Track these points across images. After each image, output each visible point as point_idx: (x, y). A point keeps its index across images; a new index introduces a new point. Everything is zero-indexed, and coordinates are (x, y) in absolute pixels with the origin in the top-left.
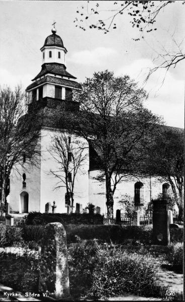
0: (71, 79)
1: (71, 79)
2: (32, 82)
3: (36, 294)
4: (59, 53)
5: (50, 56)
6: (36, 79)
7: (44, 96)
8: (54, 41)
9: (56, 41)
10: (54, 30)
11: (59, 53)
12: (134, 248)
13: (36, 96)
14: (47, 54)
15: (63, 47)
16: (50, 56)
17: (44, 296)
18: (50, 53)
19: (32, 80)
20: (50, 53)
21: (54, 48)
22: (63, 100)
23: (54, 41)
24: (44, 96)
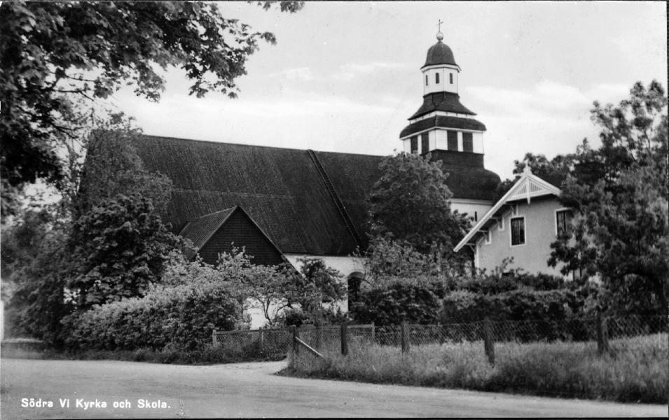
0: (469, 117)
1: (469, 117)
2: (407, 123)
3: (45, 403)
4: (451, 75)
5: (437, 81)
6: (414, 117)
7: (431, 148)
8: (440, 56)
9: (9, 295)
10: (440, 35)
11: (451, 75)
12: (415, 398)
13: (423, 142)
14: (432, 79)
15: (455, 65)
16: (437, 81)
17: (63, 405)
18: (437, 75)
19: (410, 119)
20: (437, 75)
21: (429, 69)
22: (461, 153)
23: (440, 56)
24: (431, 148)
